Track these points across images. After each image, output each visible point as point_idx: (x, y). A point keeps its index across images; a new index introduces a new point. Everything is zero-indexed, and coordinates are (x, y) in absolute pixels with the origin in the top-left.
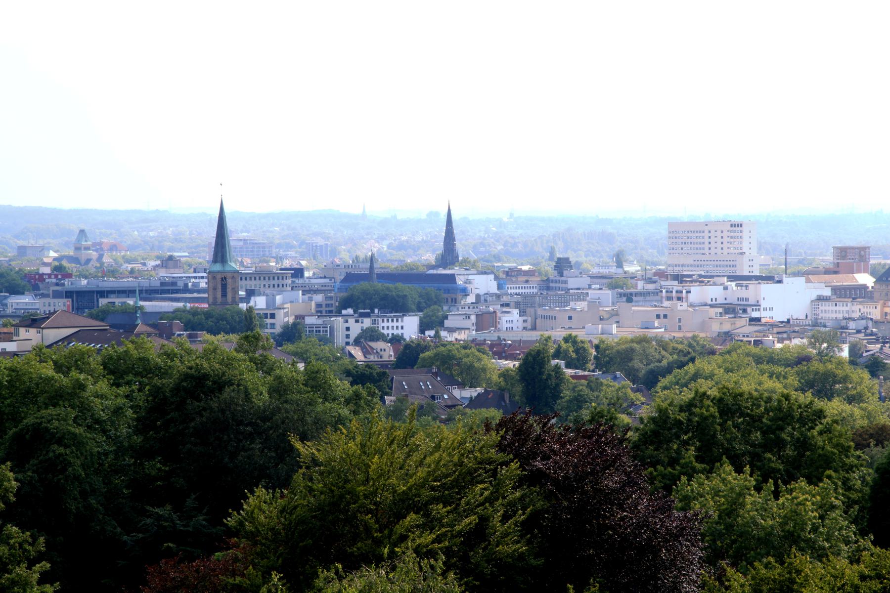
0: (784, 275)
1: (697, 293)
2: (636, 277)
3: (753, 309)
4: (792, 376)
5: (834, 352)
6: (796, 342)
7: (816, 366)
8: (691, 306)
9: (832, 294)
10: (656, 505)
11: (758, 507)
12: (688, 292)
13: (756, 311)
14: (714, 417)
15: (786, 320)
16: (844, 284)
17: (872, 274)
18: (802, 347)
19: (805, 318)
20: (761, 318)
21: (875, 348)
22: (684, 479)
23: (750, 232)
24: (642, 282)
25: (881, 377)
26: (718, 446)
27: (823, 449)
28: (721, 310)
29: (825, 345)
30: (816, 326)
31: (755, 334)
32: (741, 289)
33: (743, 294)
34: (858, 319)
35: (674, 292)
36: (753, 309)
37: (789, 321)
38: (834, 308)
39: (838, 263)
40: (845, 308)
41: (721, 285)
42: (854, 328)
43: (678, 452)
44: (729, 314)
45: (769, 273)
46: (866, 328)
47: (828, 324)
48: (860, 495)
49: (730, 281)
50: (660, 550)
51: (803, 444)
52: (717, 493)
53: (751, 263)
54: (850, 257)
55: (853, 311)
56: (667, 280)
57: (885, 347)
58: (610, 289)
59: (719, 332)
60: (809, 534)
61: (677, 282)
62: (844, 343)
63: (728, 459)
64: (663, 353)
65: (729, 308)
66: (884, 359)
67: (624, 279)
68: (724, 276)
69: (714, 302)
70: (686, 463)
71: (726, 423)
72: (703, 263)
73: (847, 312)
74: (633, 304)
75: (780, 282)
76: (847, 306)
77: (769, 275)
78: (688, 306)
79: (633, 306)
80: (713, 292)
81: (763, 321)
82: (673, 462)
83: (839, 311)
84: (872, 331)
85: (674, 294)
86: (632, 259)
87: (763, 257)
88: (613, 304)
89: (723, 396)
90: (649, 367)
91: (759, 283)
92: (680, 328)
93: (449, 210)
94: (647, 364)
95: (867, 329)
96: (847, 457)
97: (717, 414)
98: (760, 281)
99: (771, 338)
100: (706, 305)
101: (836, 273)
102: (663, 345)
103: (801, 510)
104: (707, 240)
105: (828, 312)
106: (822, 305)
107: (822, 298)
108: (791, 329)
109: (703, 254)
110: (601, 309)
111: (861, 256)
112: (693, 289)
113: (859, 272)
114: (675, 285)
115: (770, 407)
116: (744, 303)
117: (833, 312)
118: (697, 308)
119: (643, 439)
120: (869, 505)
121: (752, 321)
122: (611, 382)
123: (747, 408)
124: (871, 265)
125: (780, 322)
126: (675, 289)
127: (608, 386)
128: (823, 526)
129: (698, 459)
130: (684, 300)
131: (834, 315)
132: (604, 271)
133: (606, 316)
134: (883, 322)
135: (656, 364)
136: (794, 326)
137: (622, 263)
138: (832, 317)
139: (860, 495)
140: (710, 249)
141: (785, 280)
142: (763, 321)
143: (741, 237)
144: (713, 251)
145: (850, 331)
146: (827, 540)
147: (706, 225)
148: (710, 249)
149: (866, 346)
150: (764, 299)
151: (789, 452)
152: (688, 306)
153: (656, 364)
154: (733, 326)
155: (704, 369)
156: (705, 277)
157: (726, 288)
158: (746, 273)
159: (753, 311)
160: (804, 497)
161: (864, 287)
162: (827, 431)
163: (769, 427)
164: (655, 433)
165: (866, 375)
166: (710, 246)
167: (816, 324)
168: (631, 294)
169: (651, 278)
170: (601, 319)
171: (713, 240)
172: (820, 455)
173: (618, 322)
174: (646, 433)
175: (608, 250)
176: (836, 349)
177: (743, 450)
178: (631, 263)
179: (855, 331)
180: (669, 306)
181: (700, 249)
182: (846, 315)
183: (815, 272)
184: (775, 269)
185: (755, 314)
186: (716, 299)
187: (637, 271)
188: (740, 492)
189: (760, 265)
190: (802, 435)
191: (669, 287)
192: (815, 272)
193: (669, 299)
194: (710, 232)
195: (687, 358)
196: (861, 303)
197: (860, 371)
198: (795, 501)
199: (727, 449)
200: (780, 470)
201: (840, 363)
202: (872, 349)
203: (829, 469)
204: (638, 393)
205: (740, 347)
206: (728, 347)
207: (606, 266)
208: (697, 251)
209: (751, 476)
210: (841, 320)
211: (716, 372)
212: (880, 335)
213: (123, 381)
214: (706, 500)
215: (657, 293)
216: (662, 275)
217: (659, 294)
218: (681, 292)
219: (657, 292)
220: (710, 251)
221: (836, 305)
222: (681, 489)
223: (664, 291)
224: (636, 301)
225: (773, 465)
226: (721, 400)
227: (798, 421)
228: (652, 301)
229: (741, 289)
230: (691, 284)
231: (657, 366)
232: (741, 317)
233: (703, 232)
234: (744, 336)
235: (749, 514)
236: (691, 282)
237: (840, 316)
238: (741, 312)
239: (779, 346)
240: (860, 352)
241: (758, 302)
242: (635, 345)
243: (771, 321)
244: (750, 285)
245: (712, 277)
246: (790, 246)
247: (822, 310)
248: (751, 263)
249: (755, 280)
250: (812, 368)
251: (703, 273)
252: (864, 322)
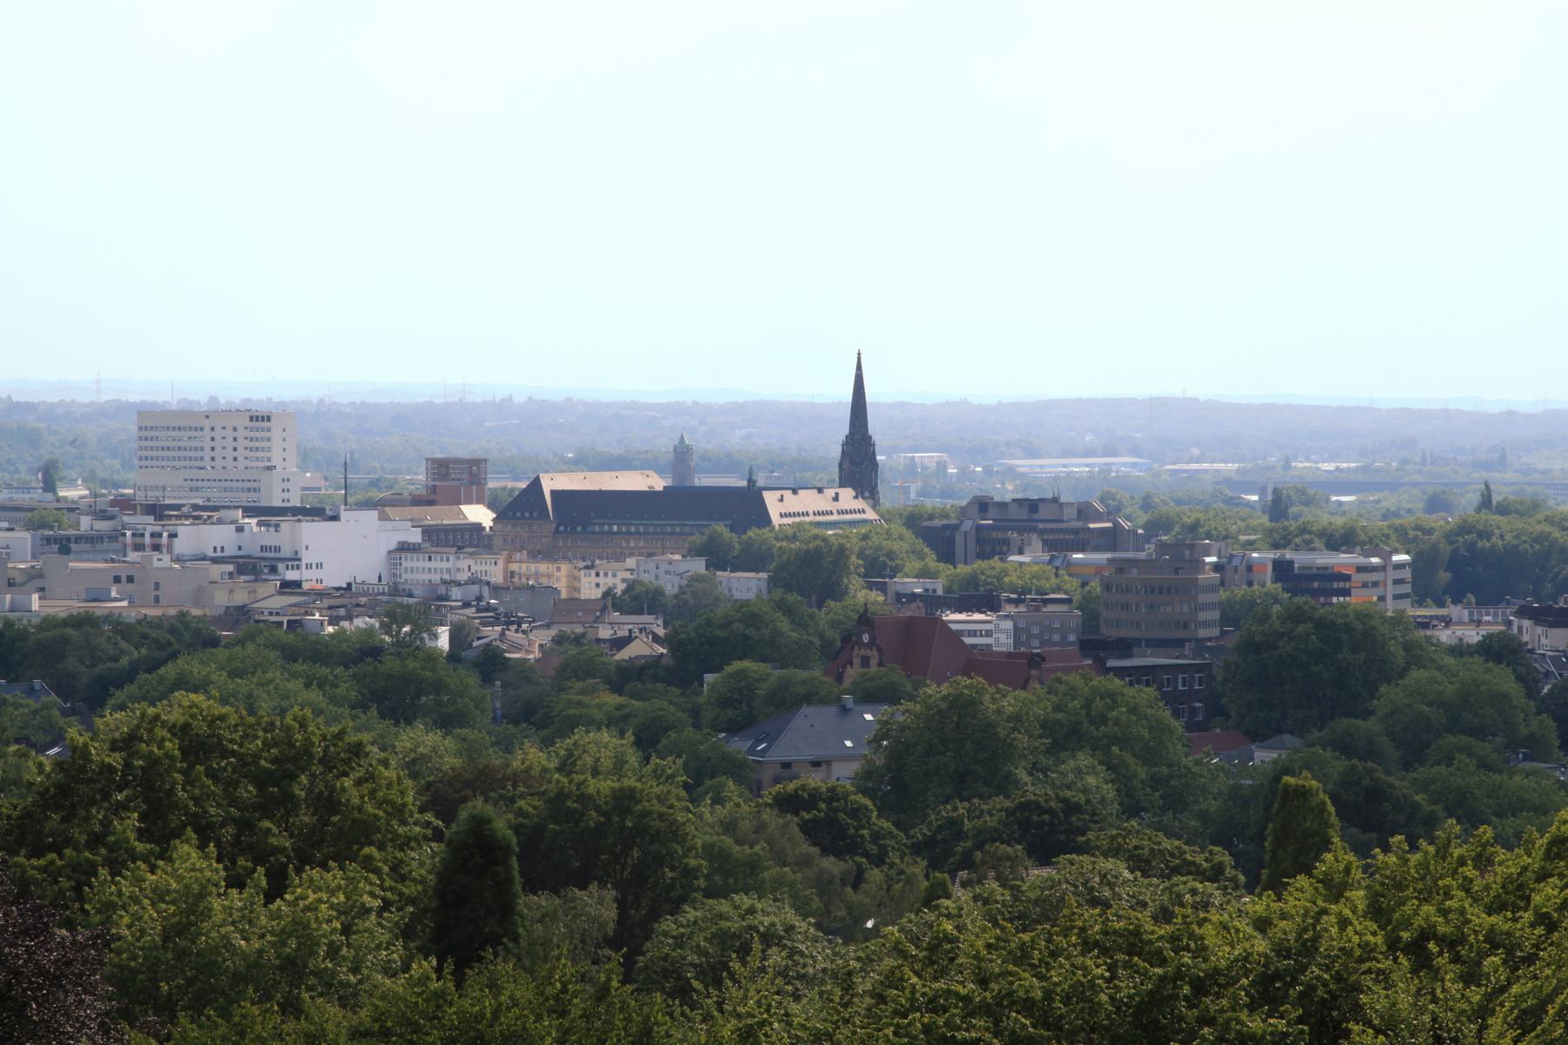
0: (342, 507)
1: (190, 538)
2: (78, 509)
3: (287, 566)
4: (346, 682)
5: (422, 639)
6: (360, 622)
7: (390, 664)
8: (178, 560)
9: (423, 540)
10: (21, 924)
11: (236, 915)
12: (173, 536)
13: (293, 568)
14: (172, 758)
15: (345, 586)
16: (445, 522)
17: (491, 507)
18: (369, 631)
19: (376, 581)
20: (301, 582)
21: (492, 632)
22: (104, 873)
23: (284, 430)
24: (90, 518)
25: (498, 683)
26: (179, 810)
27: (360, 809)
28: (230, 568)
29: (406, 629)
30: (396, 596)
31: (291, 610)
32: (268, 531)
33: (270, 538)
34: (466, 584)
35: (147, 535)
36: (287, 566)
37: (349, 585)
38: (427, 564)
39: (434, 486)
40: (445, 565)
41: (232, 523)
42: (459, 598)
43: (107, 824)
44: (244, 574)
45: (319, 502)
46: (479, 598)
47: (416, 592)
48: (420, 888)
49: (249, 517)
50: (26, 1005)
51: (327, 803)
52: (160, 895)
53: (286, 485)
54: (453, 476)
55: (458, 570)
56: (136, 513)
57: (509, 630)
58: (27, 530)
59: (227, 607)
60: (324, 961)
61: (153, 517)
62: (442, 625)
63: (195, 833)
64: (124, 644)
65: (245, 564)
66: (506, 651)
67: (56, 512)
68: (237, 507)
69: (219, 554)
70: (117, 842)
71: (194, 767)
72: (200, 484)
73: (449, 571)
74: (72, 556)
75: (335, 518)
76: (448, 560)
77: (318, 505)
78: (172, 561)
79: (71, 561)
80: (217, 537)
81: (306, 586)
82: (95, 841)
83: (436, 569)
84: (488, 603)
85: (147, 540)
86: (75, 476)
87: (308, 475)
88: (34, 556)
89: (191, 721)
90: (97, 670)
91: (299, 521)
92: (157, 600)
93: (859, 354)
94: (93, 666)
95: (481, 601)
96: (404, 823)
97: (177, 753)
98: (301, 517)
99: (317, 616)
100: (204, 558)
101: (430, 503)
102: (122, 629)
103: (309, 921)
104: (207, 445)
105: (423, 572)
106: (406, 559)
107: (406, 546)
108: (354, 601)
109: (201, 468)
110: (10, 565)
111: (471, 473)
112: (181, 530)
113: (469, 502)
114: (148, 524)
115: (273, 739)
116: (273, 555)
117: (424, 571)
118: (188, 564)
119: (42, 802)
120: (434, 905)
121: (286, 587)
122: (21, 698)
123: (232, 741)
124: (490, 489)
125: (334, 588)
126: (150, 529)
127: (17, 706)
128: (348, 946)
129: (142, 835)
130: (165, 550)
131: (427, 577)
132: (22, 498)
133: (19, 579)
134: (508, 588)
135: (110, 665)
136: (358, 595)
137: (54, 483)
138: (424, 580)
139: (420, 888)
140: (213, 459)
141: (344, 515)
142: (306, 586)
143: (269, 439)
144: (219, 463)
145: (453, 604)
146: (355, 970)
147: (207, 417)
148: (213, 459)
149: (478, 629)
150: (307, 548)
151: (305, 818)
152: (172, 561)
153: (110, 665)
154: (252, 595)
155: (191, 672)
156: (204, 509)
157: (240, 529)
158: (277, 503)
159: (287, 569)
160: (316, 896)
161: (478, 527)
162: (370, 778)
163: (269, 773)
164: (64, 790)
165: (473, 680)
166: (213, 454)
167: (395, 590)
168: (68, 539)
169: (105, 511)
170: (10, 585)
171: (218, 443)
172: (354, 821)
173: (42, 590)
174: (47, 790)
175: (30, 459)
176: (425, 635)
177: (221, 816)
178: (72, 483)
179: (460, 604)
180: (138, 560)
181: (146, 459)
182: (447, 577)
183: (395, 502)
184: (330, 496)
185: (291, 575)
186: (222, 548)
187: (82, 497)
188: (201, 893)
189: (303, 489)
190: (326, 787)
191: (139, 526)
192: (395, 502)
193: (138, 547)
194: (213, 429)
195: (164, 654)
196: (471, 554)
197: (463, 672)
198: (301, 903)
199: (195, 816)
200: (285, 849)
201: (432, 657)
202: (489, 633)
203: (369, 845)
204: (73, 718)
205: (261, 632)
206: (240, 633)
207: (26, 487)
208: (191, 463)
209: (218, 862)
210: (438, 585)
211: (214, 677)
212: (501, 609)
213: (969, 844)
214: (143, 908)
215: (117, 537)
216: (125, 504)
217: (120, 539)
218: (160, 535)
219: (116, 536)
220: (213, 464)
221: (430, 559)
222: (99, 891)
223: (128, 533)
224: (76, 552)
225: (273, 841)
226: (186, 727)
227: (321, 761)
228: (108, 551)
229: (268, 531)
230: (178, 522)
231: (110, 669)
232: (268, 580)
233: (202, 429)
234: (271, 614)
235: (218, 931)
236: (178, 517)
237: (436, 578)
238: (266, 570)
239: (330, 629)
240: (469, 640)
241: (296, 553)
242: (70, 631)
243: (319, 586)
244: (282, 524)
245: (215, 509)
246: (356, 456)
247: (406, 568)
248: (286, 485)
249: (293, 516)
250: (381, 668)
251: (200, 502)
252: (475, 588)
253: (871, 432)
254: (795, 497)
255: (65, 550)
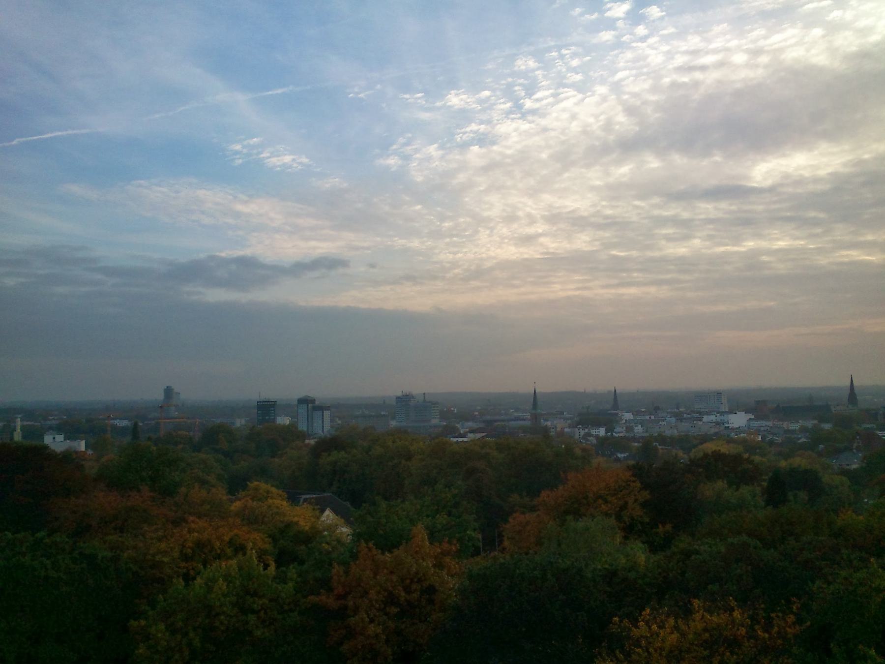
1: (706, 418)
6: (742, 435)
54: (438, 411)
80: (712, 418)
185: (727, 425)
253: (855, 392)
254: (167, 386)
255: (681, 421)
